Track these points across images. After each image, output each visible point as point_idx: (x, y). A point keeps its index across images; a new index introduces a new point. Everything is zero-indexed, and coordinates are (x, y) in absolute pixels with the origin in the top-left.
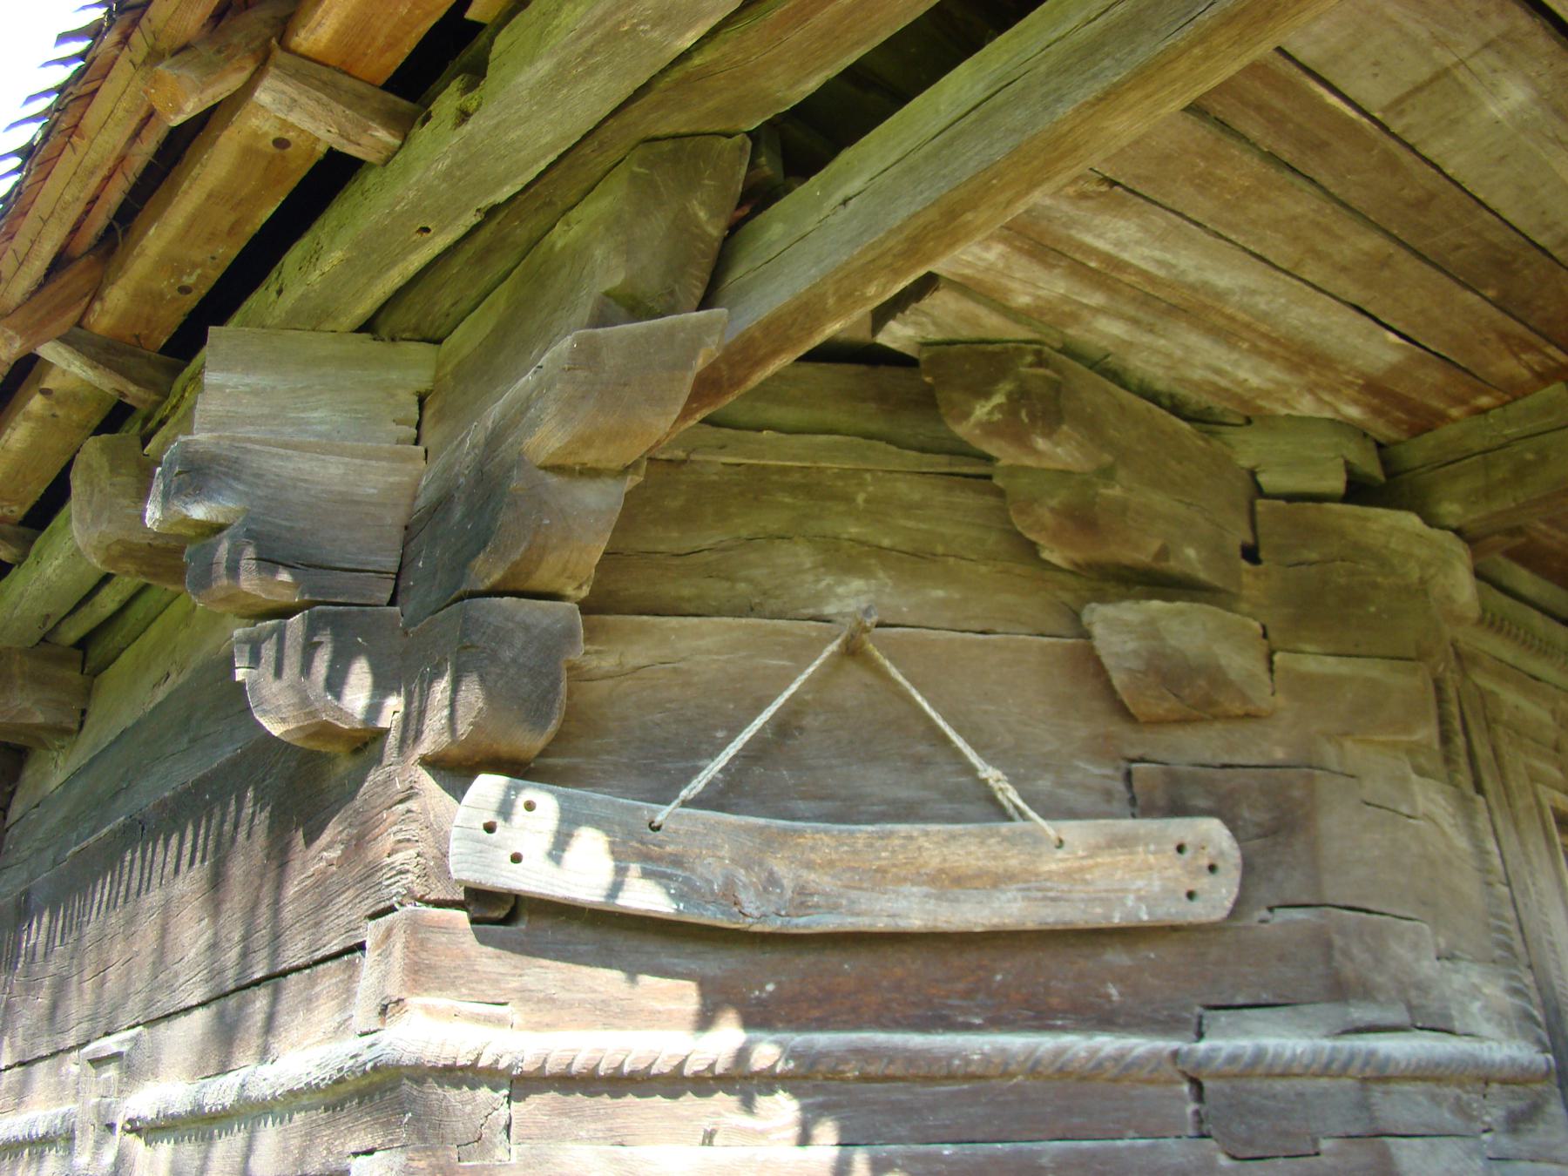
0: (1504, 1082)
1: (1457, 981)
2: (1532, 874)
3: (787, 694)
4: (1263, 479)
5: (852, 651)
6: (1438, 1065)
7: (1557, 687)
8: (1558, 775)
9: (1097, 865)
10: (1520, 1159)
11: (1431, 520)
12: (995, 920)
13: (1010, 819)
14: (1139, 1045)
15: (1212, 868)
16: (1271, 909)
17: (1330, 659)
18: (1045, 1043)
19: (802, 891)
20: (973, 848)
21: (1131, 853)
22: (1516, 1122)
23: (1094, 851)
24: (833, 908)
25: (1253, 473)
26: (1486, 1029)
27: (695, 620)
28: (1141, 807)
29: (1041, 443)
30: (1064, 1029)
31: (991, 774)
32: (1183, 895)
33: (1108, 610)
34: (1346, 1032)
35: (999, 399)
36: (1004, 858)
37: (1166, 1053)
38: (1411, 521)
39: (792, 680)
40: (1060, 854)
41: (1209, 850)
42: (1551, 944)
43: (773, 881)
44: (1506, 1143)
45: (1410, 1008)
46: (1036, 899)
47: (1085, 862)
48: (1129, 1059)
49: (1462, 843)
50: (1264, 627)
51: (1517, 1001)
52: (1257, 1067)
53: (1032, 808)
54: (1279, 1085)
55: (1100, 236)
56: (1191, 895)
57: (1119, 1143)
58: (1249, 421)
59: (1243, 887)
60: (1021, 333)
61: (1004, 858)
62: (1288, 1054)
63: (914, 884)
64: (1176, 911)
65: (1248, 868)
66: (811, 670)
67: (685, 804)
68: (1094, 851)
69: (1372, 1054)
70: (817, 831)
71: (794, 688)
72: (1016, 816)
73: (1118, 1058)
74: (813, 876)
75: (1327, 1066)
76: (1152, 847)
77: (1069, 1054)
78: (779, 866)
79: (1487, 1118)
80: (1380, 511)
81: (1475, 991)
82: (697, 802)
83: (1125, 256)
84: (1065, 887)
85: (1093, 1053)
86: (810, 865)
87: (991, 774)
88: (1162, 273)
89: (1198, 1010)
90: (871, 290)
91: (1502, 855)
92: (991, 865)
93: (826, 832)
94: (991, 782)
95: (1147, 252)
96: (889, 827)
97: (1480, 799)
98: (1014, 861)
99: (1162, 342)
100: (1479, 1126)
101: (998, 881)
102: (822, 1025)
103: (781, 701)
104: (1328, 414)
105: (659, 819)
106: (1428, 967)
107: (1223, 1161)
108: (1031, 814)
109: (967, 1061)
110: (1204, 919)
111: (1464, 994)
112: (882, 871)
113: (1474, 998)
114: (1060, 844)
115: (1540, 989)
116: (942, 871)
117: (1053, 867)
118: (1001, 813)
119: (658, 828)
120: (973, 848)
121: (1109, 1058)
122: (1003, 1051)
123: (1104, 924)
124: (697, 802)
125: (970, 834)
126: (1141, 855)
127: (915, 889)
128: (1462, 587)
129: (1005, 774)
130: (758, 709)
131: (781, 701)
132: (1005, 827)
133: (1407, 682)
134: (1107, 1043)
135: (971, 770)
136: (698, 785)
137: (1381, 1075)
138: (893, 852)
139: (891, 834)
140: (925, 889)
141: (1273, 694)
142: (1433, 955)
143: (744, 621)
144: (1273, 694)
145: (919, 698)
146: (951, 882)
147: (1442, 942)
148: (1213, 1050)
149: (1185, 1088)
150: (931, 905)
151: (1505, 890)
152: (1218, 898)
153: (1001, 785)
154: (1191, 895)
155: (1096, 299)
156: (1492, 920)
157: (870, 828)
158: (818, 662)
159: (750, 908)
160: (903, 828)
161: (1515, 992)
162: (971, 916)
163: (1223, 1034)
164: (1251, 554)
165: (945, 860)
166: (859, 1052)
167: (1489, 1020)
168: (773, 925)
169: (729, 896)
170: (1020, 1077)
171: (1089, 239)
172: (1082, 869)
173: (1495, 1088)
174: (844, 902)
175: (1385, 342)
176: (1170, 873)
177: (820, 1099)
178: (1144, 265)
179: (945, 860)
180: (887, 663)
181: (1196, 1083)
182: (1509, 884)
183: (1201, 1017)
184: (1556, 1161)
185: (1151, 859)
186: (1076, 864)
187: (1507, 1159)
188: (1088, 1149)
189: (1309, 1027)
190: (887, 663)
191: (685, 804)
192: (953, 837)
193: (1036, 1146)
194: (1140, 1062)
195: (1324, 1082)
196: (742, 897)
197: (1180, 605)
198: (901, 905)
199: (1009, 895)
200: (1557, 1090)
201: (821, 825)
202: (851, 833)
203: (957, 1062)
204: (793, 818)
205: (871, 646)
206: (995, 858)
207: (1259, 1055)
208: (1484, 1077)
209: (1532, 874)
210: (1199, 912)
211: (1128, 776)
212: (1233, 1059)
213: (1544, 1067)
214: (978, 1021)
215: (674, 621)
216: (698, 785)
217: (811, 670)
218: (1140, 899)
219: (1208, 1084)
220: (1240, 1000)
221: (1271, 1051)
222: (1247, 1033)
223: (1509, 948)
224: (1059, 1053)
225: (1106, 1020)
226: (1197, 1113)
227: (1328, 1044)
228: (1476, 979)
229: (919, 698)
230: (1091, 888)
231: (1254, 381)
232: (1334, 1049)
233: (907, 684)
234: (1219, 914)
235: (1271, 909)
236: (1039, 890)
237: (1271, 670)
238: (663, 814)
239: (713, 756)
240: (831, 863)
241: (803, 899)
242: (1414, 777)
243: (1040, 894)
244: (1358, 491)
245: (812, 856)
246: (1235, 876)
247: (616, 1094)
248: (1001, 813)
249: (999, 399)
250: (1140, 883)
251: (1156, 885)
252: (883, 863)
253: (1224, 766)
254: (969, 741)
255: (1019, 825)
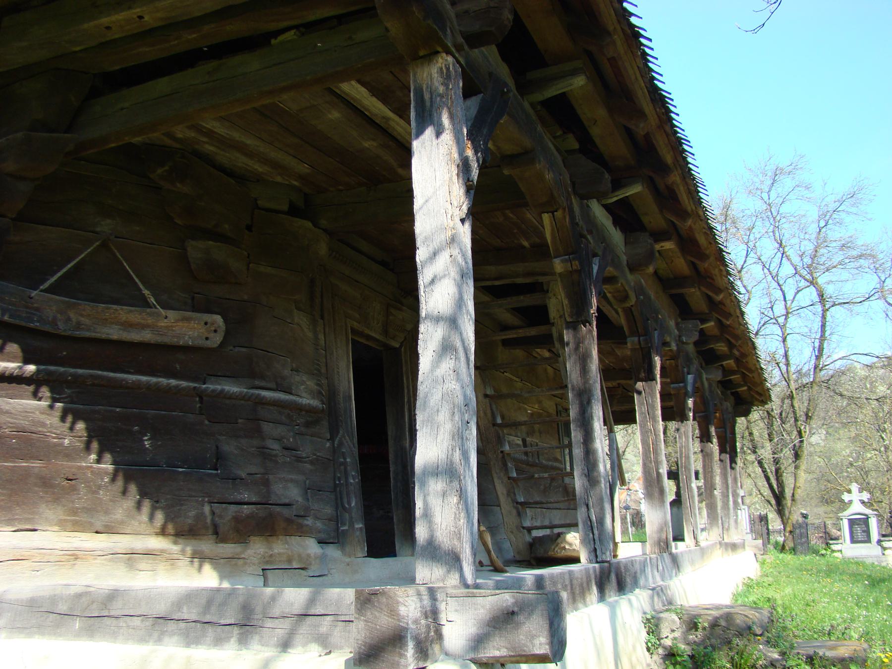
0: (307, 411)
1: (297, 378)
2: (336, 349)
3: (80, 258)
4: (259, 202)
5: (104, 245)
6: (282, 402)
7: (365, 285)
8: (358, 316)
9: (177, 325)
10: (307, 435)
11: (315, 225)
12: (141, 339)
13: (151, 308)
14: (184, 384)
15: (215, 331)
16: (234, 347)
17: (270, 268)
18: (154, 380)
19: (79, 324)
20: (137, 315)
21: (190, 323)
22: (308, 425)
23: (177, 321)
24: (89, 330)
25: (256, 200)
26: (304, 395)
27: (51, 227)
28: (195, 309)
29: (178, 185)
30: (160, 377)
31: (146, 292)
32: (204, 337)
33: (194, 243)
34: (252, 388)
35: (167, 168)
36: (147, 320)
37: (192, 387)
38: (309, 224)
39: (82, 253)
40: (166, 321)
41: (215, 325)
42: (338, 372)
43: (69, 319)
44: (303, 429)
45: (277, 384)
46: (155, 334)
47: (173, 324)
48: (180, 387)
49: (310, 335)
50: (249, 254)
51: (318, 388)
52: (222, 394)
53: (158, 305)
54: (228, 402)
55: (207, 124)
56: (207, 339)
57: (173, 413)
58: (258, 181)
59: (225, 338)
60: (178, 146)
61: (147, 320)
62: (231, 392)
63: (116, 325)
64: (201, 343)
65: (227, 333)
66: (89, 250)
67: (41, 291)
68: (177, 321)
69: (259, 395)
70: (86, 304)
71: (83, 256)
72: (153, 307)
73: (177, 386)
74: (83, 319)
75: (244, 397)
76: (196, 322)
77: (160, 384)
78: (72, 314)
79: (298, 421)
80: (298, 219)
81: (303, 383)
82: (46, 291)
83: (215, 130)
84: (166, 331)
85: (168, 384)
86: (82, 315)
87: (146, 292)
88: (228, 136)
89: (205, 375)
90: (127, 138)
91: (325, 341)
92: (142, 321)
93: (89, 305)
94: (146, 295)
95: (222, 130)
96: (110, 306)
97: (321, 321)
98: (150, 321)
99: (228, 154)
100: (295, 423)
101: (144, 327)
102: (81, 367)
103: (77, 260)
104: (287, 183)
105: (33, 295)
106: (287, 372)
107: (207, 422)
108: (158, 307)
109: (127, 383)
110: (210, 346)
111: (299, 382)
112: (106, 320)
113: (302, 385)
114: (166, 317)
115: (328, 386)
116: (125, 322)
117: (163, 324)
118: (148, 305)
119: (31, 298)
120: (137, 315)
121: (173, 386)
122: (139, 381)
123: (177, 344)
124: (46, 291)
125: (137, 311)
126: (192, 324)
127: (116, 327)
128: (323, 249)
129: (151, 292)
130: (69, 262)
131: (77, 260)
132: (148, 310)
133: (816, 244)
134: (173, 382)
135: (140, 290)
136: (46, 285)
137: (262, 402)
138: (111, 314)
139: (109, 308)
140: (119, 327)
141: (247, 277)
142: (290, 369)
143: (67, 230)
144: (247, 277)
145: (125, 264)
146: (128, 326)
147: (294, 365)
148: (207, 388)
149: (197, 399)
150: (121, 332)
151: (324, 352)
152: (216, 340)
153: (150, 296)
154: (207, 339)
155: (205, 139)
156: (316, 361)
157: (103, 305)
158: (92, 248)
159: (61, 327)
160: (115, 307)
161: (318, 385)
162: (133, 337)
163: (212, 384)
164: (249, 228)
165: (127, 318)
166: (91, 376)
167: (306, 392)
168: (69, 333)
169: (54, 322)
170: (144, 390)
171: (204, 124)
172: (172, 326)
173: (304, 413)
174: (92, 328)
175: (305, 167)
176: (201, 331)
177: (77, 390)
178: (223, 134)
179: (127, 318)
180: (116, 251)
181: (201, 398)
182: (325, 351)
183: (205, 378)
184: (320, 438)
185: (196, 325)
186: (171, 324)
187: (303, 434)
188: (72, 267)
189: (240, 385)
190: (116, 251)
191: (41, 291)
192: (131, 311)
193: (147, 411)
194: (184, 389)
195: (243, 402)
196: (59, 323)
197: (218, 244)
198: (111, 331)
199: (147, 332)
200: (327, 418)
201: (87, 303)
202: (97, 306)
203: (124, 382)
204: (78, 299)
205: (111, 245)
206: (144, 320)
207: (222, 391)
208: (300, 409)
209: (336, 349)
210: (208, 344)
211: (193, 298)
212: (213, 391)
213: (321, 408)
214: (132, 371)
215: (42, 227)
216: (46, 285)
217: (89, 250)
218: (190, 338)
219: (205, 398)
220: (219, 374)
221: (226, 390)
222: (220, 384)
223: (319, 371)
224: (157, 383)
225: (174, 376)
226: (200, 407)
227: (245, 390)
228: (305, 379)
229: (125, 264)
230: (174, 333)
231: (260, 170)
232: (247, 392)
233: (121, 259)
234: (215, 345)
235: (234, 347)
236: (157, 331)
237: (248, 269)
238: (34, 293)
239: (52, 276)
240: (89, 315)
241: (78, 326)
242: (295, 310)
243: (157, 333)
244: (294, 211)
245: (83, 313)
246: (223, 334)
247: (10, 383)
248: (148, 305)
249: (167, 168)
250: (191, 333)
251: (196, 334)
252: (107, 317)
253: (226, 299)
254: (140, 280)
255: (154, 310)
